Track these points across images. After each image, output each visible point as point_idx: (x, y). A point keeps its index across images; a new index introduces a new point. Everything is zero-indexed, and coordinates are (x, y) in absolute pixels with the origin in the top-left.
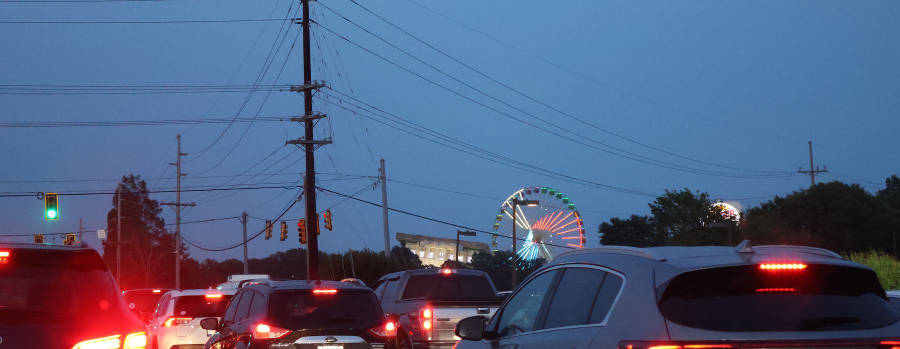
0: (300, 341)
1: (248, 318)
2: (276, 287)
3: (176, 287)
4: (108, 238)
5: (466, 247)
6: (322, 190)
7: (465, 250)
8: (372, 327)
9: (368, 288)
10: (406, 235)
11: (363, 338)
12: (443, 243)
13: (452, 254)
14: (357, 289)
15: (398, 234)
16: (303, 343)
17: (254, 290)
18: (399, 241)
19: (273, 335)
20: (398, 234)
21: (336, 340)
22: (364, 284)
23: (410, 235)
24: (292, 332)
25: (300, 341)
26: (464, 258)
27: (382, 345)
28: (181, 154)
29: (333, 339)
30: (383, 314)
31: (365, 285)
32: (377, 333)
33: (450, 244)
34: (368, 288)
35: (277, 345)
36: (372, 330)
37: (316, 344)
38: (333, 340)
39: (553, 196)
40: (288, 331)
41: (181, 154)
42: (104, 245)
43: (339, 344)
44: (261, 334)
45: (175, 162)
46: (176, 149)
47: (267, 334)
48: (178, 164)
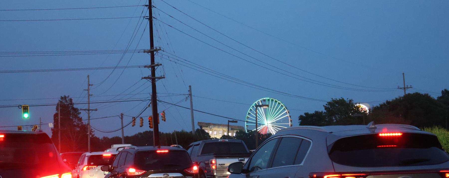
1: (124, 165)
2: (138, 150)
5: (233, 128)
7: (232, 130)
9: (184, 149)
10: (202, 123)
12: (221, 126)
21: (168, 175)
26: (232, 134)
29: (167, 175)
32: (189, 171)
33: (225, 127)
34: (184, 149)
47: (134, 173)
48: (88, 90)
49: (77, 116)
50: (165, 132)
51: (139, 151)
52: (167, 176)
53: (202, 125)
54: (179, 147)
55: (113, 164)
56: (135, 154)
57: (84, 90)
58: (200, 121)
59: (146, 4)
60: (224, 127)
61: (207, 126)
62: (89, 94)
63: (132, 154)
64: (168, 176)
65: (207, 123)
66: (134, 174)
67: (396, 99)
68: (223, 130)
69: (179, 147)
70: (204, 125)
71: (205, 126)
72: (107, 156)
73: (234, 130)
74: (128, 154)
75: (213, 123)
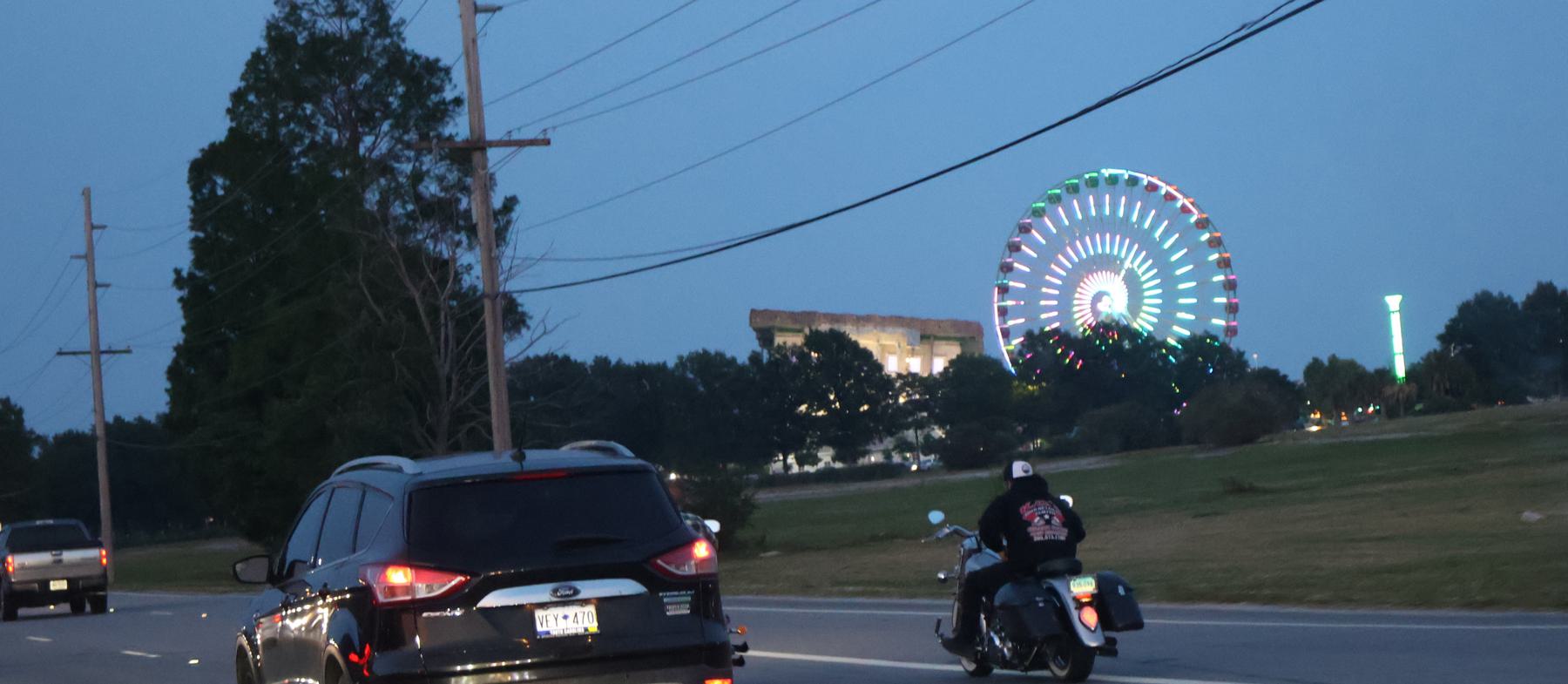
0: (492, 600)
1: (354, 551)
2: (420, 474)
3: (497, 439)
4: (198, 263)
5: (928, 332)
6: (99, 407)
7: (925, 341)
8: (660, 554)
9: (639, 462)
10: (773, 314)
11: (646, 587)
12: (870, 327)
13: (894, 353)
14: (623, 466)
15: (753, 312)
16: (512, 604)
17: (362, 484)
18: (755, 329)
19: (422, 592)
20: (753, 312)
21: (576, 592)
22: (628, 453)
23: (785, 312)
24: (470, 580)
25: (492, 600)
26: (923, 362)
27: (688, 595)
28: (93, 227)
29: (570, 589)
30: (682, 521)
31: (632, 455)
32: (672, 569)
33: (890, 329)
34: (639, 462)
35: (445, 614)
36: (659, 562)
37: (532, 604)
38: (568, 592)
39: (1135, 189)
40: (460, 578)
41: (93, 227)
42: (181, 288)
43: (585, 602)
44: (392, 590)
45: (83, 250)
46: (82, 219)
47: (408, 589)
48: (89, 257)
49: (357, 71)
50: (1127, 302)
51: (424, 478)
52: (567, 596)
53: (770, 324)
54: (612, 452)
55: (287, 547)
56: (406, 496)
57: (74, 261)
58: (761, 306)
59: (100, 231)
60: (884, 331)
61: (798, 326)
62: (96, 283)
63: (393, 498)
64: (574, 598)
65: (798, 314)
66: (407, 594)
67: (140, 419)
68: (881, 345)
69: (612, 452)
70: (784, 326)
71: (790, 326)
72: (922, 670)
73: (936, 342)
74: (367, 495)
75: (830, 310)
